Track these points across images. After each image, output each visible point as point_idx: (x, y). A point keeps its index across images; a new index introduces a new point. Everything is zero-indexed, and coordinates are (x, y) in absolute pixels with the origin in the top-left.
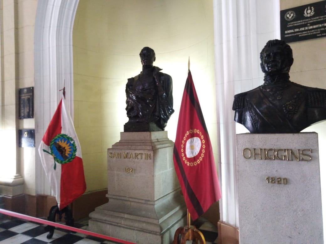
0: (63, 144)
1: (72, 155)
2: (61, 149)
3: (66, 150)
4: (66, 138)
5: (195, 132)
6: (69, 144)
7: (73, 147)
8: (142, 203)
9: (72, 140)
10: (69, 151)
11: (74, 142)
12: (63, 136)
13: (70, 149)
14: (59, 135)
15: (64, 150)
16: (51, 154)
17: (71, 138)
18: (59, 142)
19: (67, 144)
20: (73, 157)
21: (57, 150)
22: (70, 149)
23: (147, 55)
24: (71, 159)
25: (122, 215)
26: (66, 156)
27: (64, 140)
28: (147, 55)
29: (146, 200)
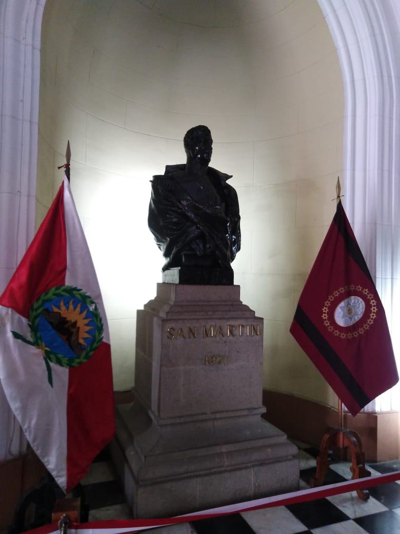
0: (72, 314)
1: (94, 340)
2: (66, 326)
3: (79, 328)
4: (79, 297)
5: (352, 289)
6: (85, 313)
7: (95, 319)
8: (243, 416)
9: (92, 302)
10: (87, 332)
11: (96, 309)
12: (71, 291)
13: (87, 325)
14: (57, 289)
15: (74, 330)
16: (34, 344)
17: (89, 297)
18: (59, 308)
19: (81, 312)
20: (95, 345)
21: (53, 332)
22: (87, 325)
23: (199, 141)
24: (91, 350)
25: (218, 449)
26: (80, 344)
27: (73, 303)
28: (199, 141)
29: (249, 409)
